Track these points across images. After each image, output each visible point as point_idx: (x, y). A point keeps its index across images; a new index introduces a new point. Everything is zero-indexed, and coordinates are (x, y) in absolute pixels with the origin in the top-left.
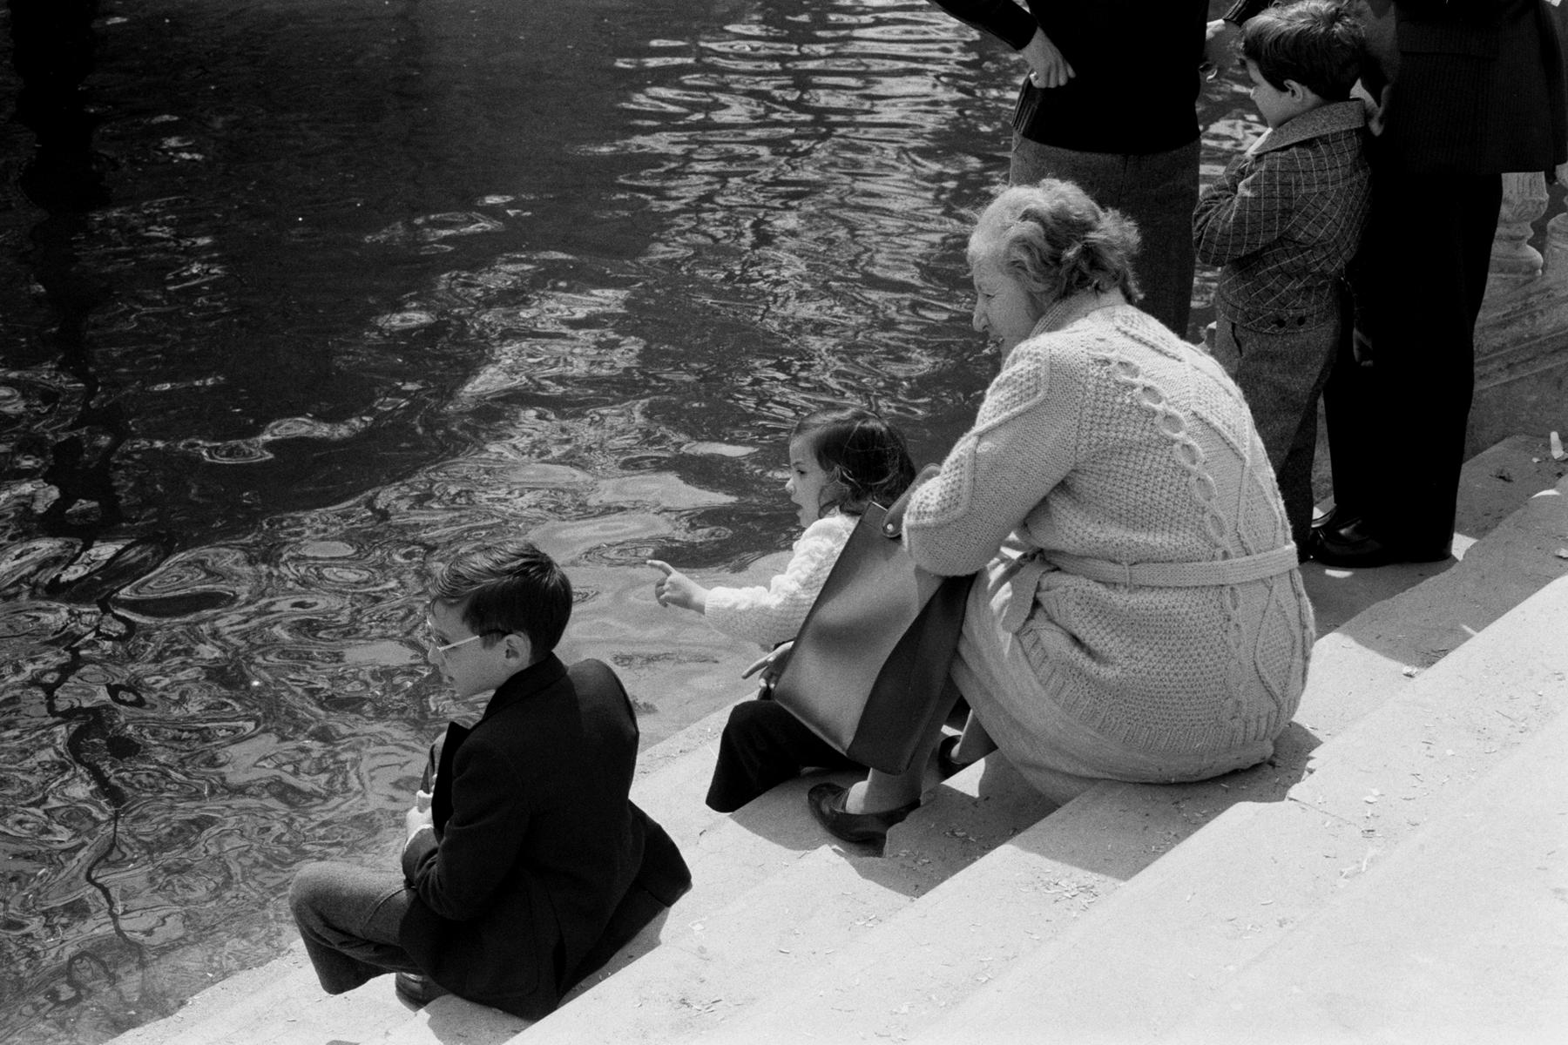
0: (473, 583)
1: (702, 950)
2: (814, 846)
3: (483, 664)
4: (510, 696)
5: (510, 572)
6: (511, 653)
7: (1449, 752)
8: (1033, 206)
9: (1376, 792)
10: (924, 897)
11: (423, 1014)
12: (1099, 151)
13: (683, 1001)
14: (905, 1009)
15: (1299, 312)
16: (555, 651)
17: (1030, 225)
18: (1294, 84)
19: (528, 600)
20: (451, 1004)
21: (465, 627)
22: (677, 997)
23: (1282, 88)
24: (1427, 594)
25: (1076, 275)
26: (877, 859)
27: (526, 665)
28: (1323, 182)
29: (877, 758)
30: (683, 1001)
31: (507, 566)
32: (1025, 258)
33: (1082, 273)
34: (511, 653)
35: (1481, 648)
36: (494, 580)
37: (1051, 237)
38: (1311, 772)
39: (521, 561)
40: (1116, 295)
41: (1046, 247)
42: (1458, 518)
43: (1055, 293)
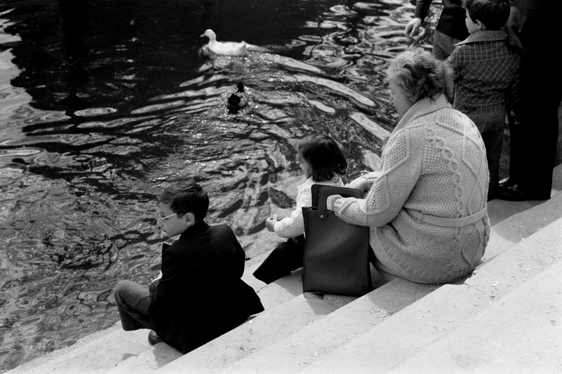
0: (174, 195)
1: (251, 330)
2: (297, 294)
3: (172, 225)
4: (187, 234)
5: (187, 191)
6: (188, 220)
7: (528, 269)
8: (408, 63)
9: (498, 283)
10: (332, 314)
11: (153, 348)
12: (521, 42)
13: (241, 348)
14: (316, 354)
15: (473, 105)
16: (204, 220)
17: (406, 70)
18: (479, 22)
19: (192, 201)
20: (163, 345)
21: (171, 211)
22: (239, 346)
23: (475, 22)
24: (534, 212)
25: (423, 91)
26: (321, 300)
27: (193, 224)
28: (474, 59)
30: (241, 348)
31: (186, 188)
32: (403, 83)
33: (425, 90)
34: (188, 220)
35: (542, 234)
36: (186, 193)
37: (413, 75)
38: (475, 274)
39: (191, 187)
40: (442, 99)
41: (412, 79)
42: (553, 186)
43: (416, 97)
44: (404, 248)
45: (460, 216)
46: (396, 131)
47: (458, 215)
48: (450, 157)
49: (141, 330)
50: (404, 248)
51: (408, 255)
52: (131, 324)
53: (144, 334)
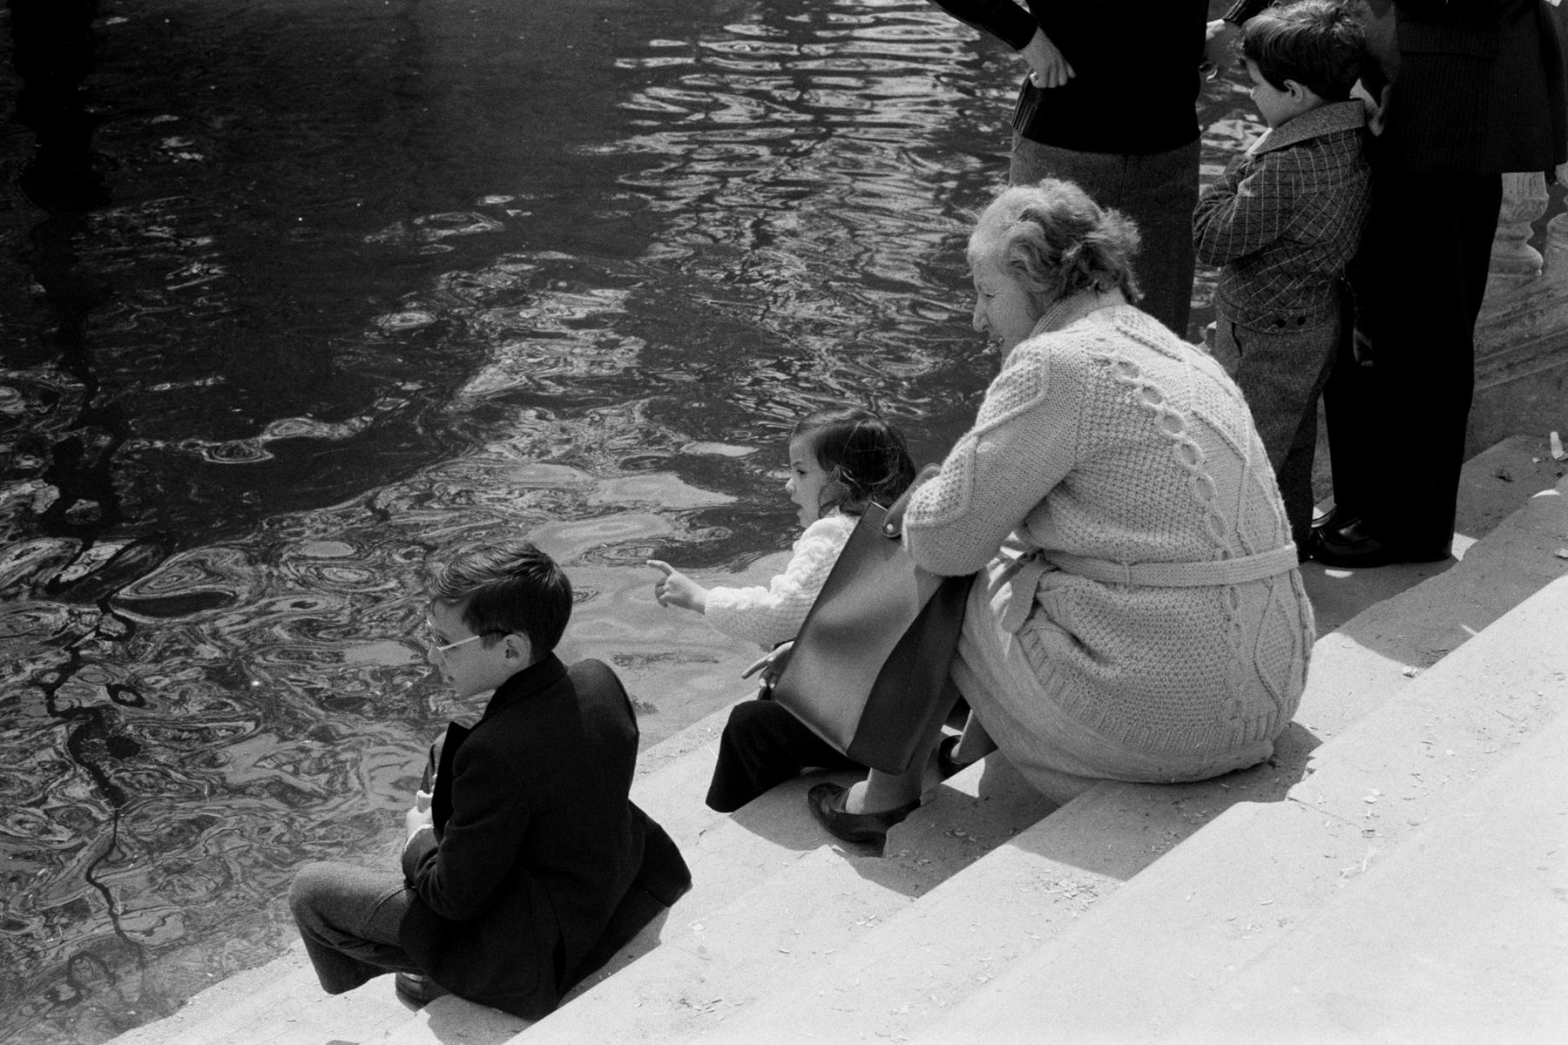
0: (473, 583)
1: (702, 950)
2: (814, 846)
3: (483, 664)
4: (510, 696)
5: (510, 572)
6: (511, 653)
7: (1449, 752)
8: (1033, 206)
9: (1376, 792)
10: (924, 897)
11: (423, 1014)
13: (683, 1001)
14: (905, 1009)
15: (1299, 312)
16: (555, 651)
17: (1030, 225)
18: (1294, 84)
19: (528, 600)
20: (451, 1004)
21: (465, 627)
22: (677, 997)
23: (1282, 88)
24: (1427, 594)
25: (1076, 275)
26: (877, 859)
27: (526, 665)
28: (1323, 182)
29: (877, 758)
30: (683, 1001)
31: (507, 566)
32: (1025, 258)
33: (1082, 273)
34: (511, 653)
35: (1481, 648)
36: (494, 580)
37: (1051, 237)
38: (1311, 772)
39: (521, 561)
40: (1116, 295)
41: (1046, 247)
42: (1458, 518)
43: (1055, 293)
44: (1108, 673)
45: (1226, 555)
46: (587, 539)
47: (1219, 552)
48: (1194, 462)
49: (372, 981)
50: (1108, 673)
51: (1118, 691)
52: (342, 969)
53: (383, 986)
